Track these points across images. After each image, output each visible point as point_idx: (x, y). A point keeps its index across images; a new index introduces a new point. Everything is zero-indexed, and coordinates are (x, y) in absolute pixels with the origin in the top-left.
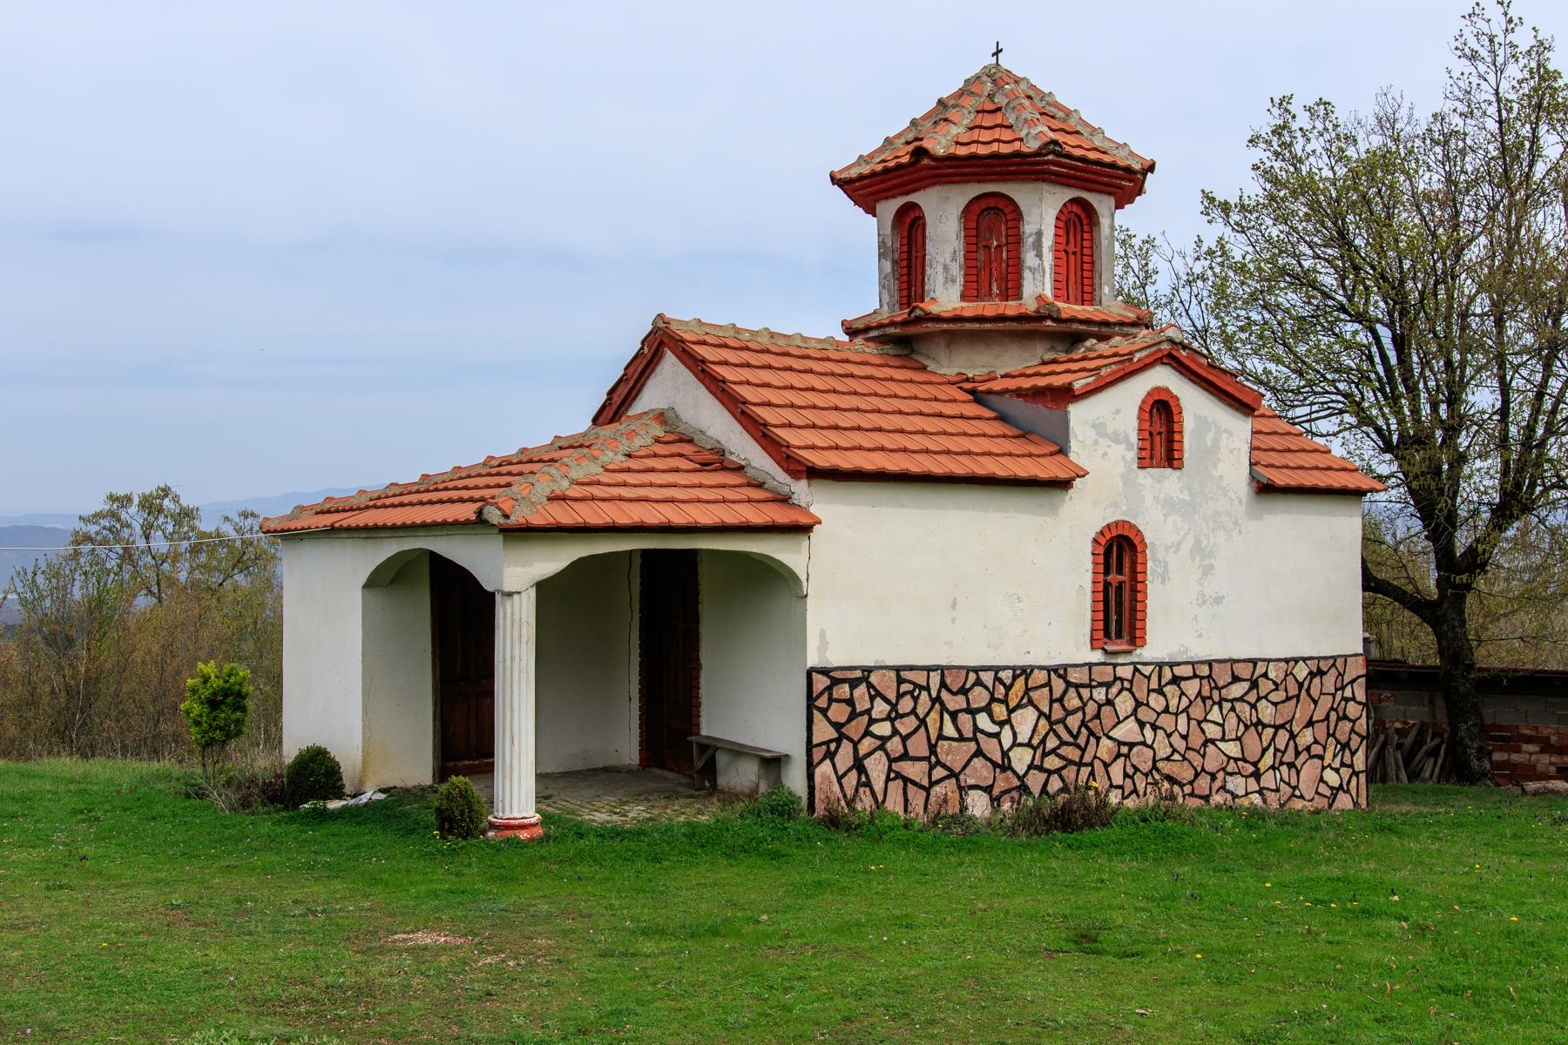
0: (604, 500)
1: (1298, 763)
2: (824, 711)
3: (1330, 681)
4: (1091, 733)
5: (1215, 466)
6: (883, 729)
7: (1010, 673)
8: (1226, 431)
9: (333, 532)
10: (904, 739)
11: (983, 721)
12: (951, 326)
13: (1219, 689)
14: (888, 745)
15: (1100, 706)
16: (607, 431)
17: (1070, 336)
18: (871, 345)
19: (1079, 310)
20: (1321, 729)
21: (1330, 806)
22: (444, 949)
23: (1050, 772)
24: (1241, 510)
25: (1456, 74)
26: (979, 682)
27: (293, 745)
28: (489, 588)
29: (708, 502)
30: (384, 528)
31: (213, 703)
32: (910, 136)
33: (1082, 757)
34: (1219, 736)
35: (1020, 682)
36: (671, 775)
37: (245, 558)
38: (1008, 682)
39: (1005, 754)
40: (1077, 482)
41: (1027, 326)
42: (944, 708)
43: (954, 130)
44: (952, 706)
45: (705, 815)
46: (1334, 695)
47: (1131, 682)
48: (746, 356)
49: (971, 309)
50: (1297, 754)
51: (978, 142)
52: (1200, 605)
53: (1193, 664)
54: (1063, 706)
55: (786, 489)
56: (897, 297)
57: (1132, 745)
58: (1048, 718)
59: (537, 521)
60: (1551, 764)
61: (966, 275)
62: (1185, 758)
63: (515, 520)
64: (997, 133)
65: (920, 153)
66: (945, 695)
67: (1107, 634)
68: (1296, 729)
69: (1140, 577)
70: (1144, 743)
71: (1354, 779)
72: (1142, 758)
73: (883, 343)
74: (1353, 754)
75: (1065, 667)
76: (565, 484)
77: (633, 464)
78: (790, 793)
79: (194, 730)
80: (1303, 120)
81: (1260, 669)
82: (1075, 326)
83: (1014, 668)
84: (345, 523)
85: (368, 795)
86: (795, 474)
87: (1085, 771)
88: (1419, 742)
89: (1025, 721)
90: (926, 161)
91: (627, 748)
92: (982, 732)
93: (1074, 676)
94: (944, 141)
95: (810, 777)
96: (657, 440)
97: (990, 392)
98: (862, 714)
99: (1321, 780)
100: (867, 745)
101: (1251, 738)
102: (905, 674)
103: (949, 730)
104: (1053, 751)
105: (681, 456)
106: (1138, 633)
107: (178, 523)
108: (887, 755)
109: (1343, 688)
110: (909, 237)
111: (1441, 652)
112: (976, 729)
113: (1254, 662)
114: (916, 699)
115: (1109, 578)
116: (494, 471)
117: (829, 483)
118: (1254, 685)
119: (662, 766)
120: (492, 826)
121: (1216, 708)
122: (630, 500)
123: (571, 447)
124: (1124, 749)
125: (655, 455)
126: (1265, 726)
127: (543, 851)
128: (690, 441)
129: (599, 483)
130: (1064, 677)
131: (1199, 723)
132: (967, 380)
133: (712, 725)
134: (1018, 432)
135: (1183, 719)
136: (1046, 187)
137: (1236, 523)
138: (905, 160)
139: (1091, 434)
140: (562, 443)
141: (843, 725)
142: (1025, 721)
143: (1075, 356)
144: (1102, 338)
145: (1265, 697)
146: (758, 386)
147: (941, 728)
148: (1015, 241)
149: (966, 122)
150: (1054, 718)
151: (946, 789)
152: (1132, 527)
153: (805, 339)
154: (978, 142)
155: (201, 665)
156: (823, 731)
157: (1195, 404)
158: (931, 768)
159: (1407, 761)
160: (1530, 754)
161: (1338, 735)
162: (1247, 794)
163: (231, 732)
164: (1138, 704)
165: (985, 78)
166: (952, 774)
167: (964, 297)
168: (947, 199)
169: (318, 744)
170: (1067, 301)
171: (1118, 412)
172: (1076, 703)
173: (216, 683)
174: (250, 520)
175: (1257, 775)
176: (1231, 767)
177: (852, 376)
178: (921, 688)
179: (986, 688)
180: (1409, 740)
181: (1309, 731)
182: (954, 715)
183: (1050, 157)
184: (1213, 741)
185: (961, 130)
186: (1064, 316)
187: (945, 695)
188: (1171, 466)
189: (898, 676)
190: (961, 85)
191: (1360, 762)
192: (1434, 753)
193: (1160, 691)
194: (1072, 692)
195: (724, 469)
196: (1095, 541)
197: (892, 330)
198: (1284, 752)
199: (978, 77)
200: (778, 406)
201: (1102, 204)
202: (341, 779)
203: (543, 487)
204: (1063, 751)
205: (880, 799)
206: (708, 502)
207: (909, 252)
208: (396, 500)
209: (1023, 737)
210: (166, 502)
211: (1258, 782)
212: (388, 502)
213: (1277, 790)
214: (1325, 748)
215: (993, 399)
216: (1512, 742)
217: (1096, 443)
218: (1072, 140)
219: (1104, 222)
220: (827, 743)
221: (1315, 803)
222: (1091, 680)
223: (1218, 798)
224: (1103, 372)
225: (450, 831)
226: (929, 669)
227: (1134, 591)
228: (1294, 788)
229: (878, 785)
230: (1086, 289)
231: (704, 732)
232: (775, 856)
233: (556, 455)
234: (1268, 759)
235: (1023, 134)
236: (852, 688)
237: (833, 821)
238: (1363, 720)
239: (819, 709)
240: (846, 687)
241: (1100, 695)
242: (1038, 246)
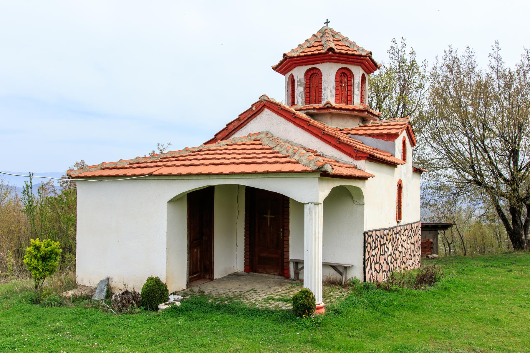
56: (304, 101)
119: (256, 272)
168: (331, 68)
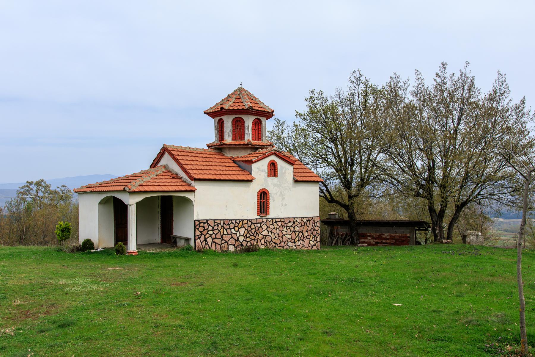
0: (150, 185)
1: (304, 240)
2: (198, 229)
3: (311, 222)
4: (257, 233)
5: (285, 177)
6: (211, 232)
7: (239, 221)
8: (287, 169)
9: (91, 192)
10: (215, 235)
11: (233, 231)
12: (229, 146)
13: (286, 224)
14: (212, 236)
15: (259, 228)
16: (153, 170)
17: (255, 148)
18: (212, 150)
19: (257, 143)
20: (309, 233)
21: (311, 249)
22: (118, 269)
23: (248, 242)
24: (291, 186)
25: (349, 86)
26: (232, 223)
27: (81, 240)
28: (126, 204)
29: (173, 186)
30: (103, 191)
31: (63, 231)
32: (221, 103)
33: (255, 238)
34: (286, 234)
35: (241, 223)
36: (167, 244)
37: (63, 197)
38: (238, 223)
39: (238, 238)
40: (253, 180)
41: (246, 146)
42: (224, 228)
43: (230, 103)
44: (226, 228)
45: (172, 250)
46: (312, 225)
47: (266, 222)
48: (183, 153)
49: (234, 142)
50: (304, 238)
51: (235, 106)
52: (282, 206)
53: (280, 219)
54: (251, 228)
55: (190, 183)
57: (266, 236)
58: (247, 230)
59: (136, 190)
60: (374, 242)
61: (233, 135)
62: (278, 239)
63: (131, 190)
64: (239, 104)
65: (222, 108)
66: (224, 225)
67: (261, 212)
68: (304, 232)
69: (268, 200)
70: (269, 235)
71: (317, 243)
72: (269, 239)
73: (215, 149)
74: (317, 238)
75: (251, 219)
76: (142, 182)
77: (157, 177)
78: (191, 246)
79: (58, 237)
80: (316, 96)
81: (295, 219)
82: (256, 146)
83: (240, 220)
84: (94, 190)
85: (100, 249)
86: (192, 180)
87: (256, 241)
88: (346, 237)
89: (242, 231)
90: (224, 110)
91: (158, 239)
92: (233, 233)
93: (253, 221)
94: (228, 106)
95: (195, 242)
96: (163, 172)
97: (237, 161)
98: (206, 229)
99: (310, 243)
100: (207, 236)
101: (293, 234)
102: (216, 221)
103: (225, 233)
104: (249, 237)
105: (168, 175)
106: (268, 212)
107: (45, 188)
108: (212, 238)
109: (315, 224)
110: (221, 126)
111: (349, 217)
112: (231, 232)
113: (294, 218)
114: (218, 226)
115: (261, 201)
116: (127, 178)
117: (199, 181)
118: (294, 223)
120: (127, 252)
121: (285, 228)
122: (156, 185)
123: (145, 173)
124: (264, 237)
125: (162, 175)
126: (296, 232)
127: (138, 257)
128: (171, 172)
129: (150, 182)
130: (251, 222)
131: (281, 231)
132: (233, 158)
133: (176, 233)
134: (242, 170)
135: (278, 230)
136: (250, 116)
137: (290, 189)
138: (219, 109)
139: (257, 170)
140: (143, 172)
141: (202, 232)
142: (242, 231)
143: (256, 153)
144: (262, 149)
145: (297, 226)
146: (185, 160)
147: (224, 232)
148: (243, 127)
149: (233, 101)
150: (249, 230)
151: (225, 245)
152: (266, 189)
153: (197, 149)
154: (235, 106)
155: (59, 222)
156: (198, 233)
157: (280, 163)
158: (221, 241)
159: (343, 242)
160: (369, 239)
161: (313, 234)
162: (292, 246)
163: (67, 238)
164: (268, 227)
165: (238, 90)
166: (226, 242)
167: (232, 140)
168: (228, 118)
169: (89, 238)
170: (255, 140)
171: (263, 165)
172: (254, 227)
173: (63, 226)
174: (64, 188)
175: (295, 242)
176: (289, 240)
177: (207, 157)
178: (219, 224)
179: (233, 224)
180: (343, 237)
181: (306, 233)
182: (226, 230)
183: (250, 110)
184: (285, 235)
185: (232, 103)
186: (253, 144)
187: (224, 225)
188: (275, 177)
189: (214, 221)
190: (233, 92)
191: (318, 239)
192: (349, 240)
193: (273, 224)
194: (253, 225)
195: (177, 178)
196: (258, 193)
197: (217, 147)
198: (301, 237)
199: (236, 90)
200: (189, 165)
201: (263, 119)
202: (94, 246)
203: (138, 183)
204: (251, 237)
205: (210, 247)
206: (173, 186)
207: (221, 129)
208: (106, 185)
209: (242, 234)
210: (42, 183)
211: (295, 244)
212: (104, 185)
213: (299, 245)
214: (310, 237)
215: (238, 163)
216: (365, 237)
217: (258, 172)
218: (256, 105)
219: (263, 123)
220: (199, 235)
221: (308, 248)
222: (257, 222)
223: (285, 247)
224: (259, 157)
225: (119, 253)
226: (221, 220)
227: (267, 203)
228: (304, 245)
229: (210, 244)
230: (259, 138)
231: (174, 234)
232: (185, 257)
233: (141, 175)
234: (297, 239)
235: (245, 104)
236: (204, 224)
237: (199, 251)
238: (319, 230)
239: (197, 228)
240: (203, 224)
241: (259, 225)
242: (248, 129)
